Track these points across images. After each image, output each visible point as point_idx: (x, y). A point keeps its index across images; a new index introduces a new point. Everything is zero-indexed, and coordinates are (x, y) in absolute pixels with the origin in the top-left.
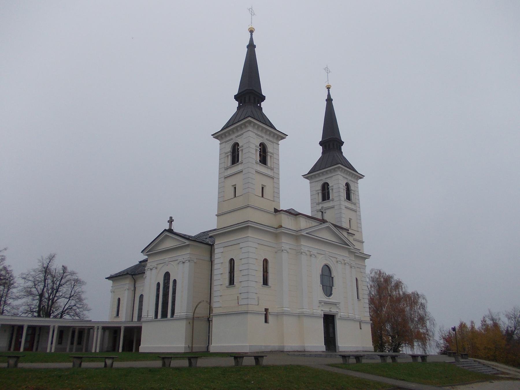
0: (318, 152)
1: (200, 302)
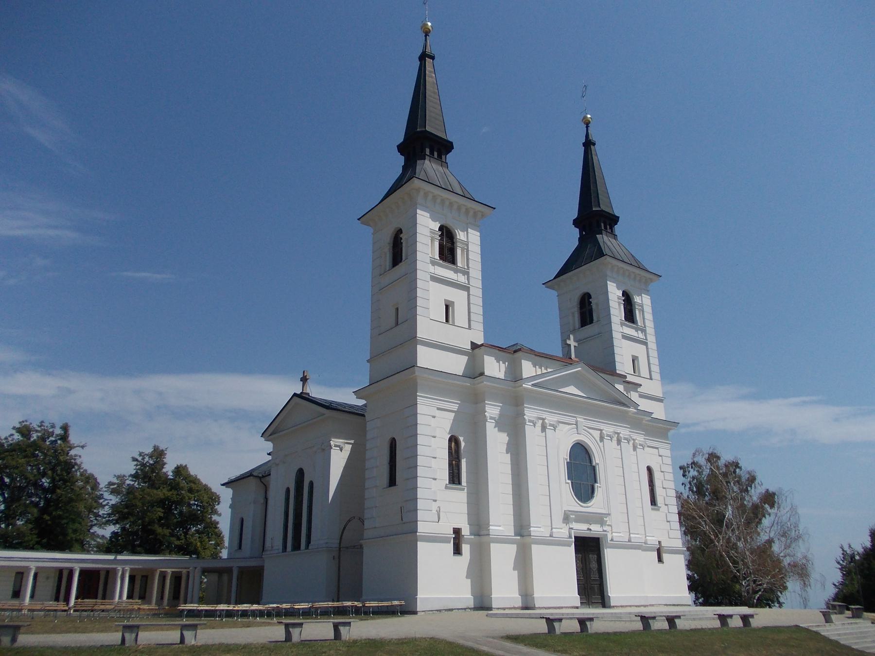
0: (572, 238)
1: (349, 521)
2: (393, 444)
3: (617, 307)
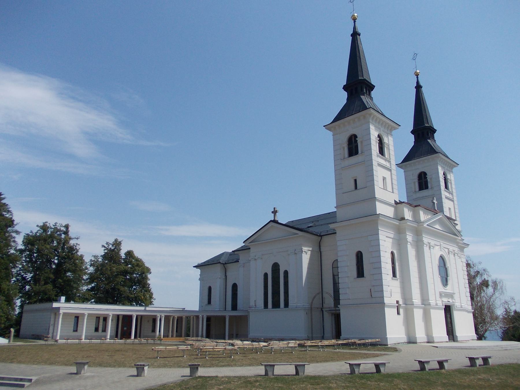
2: (359, 256)
3: (375, 145)
